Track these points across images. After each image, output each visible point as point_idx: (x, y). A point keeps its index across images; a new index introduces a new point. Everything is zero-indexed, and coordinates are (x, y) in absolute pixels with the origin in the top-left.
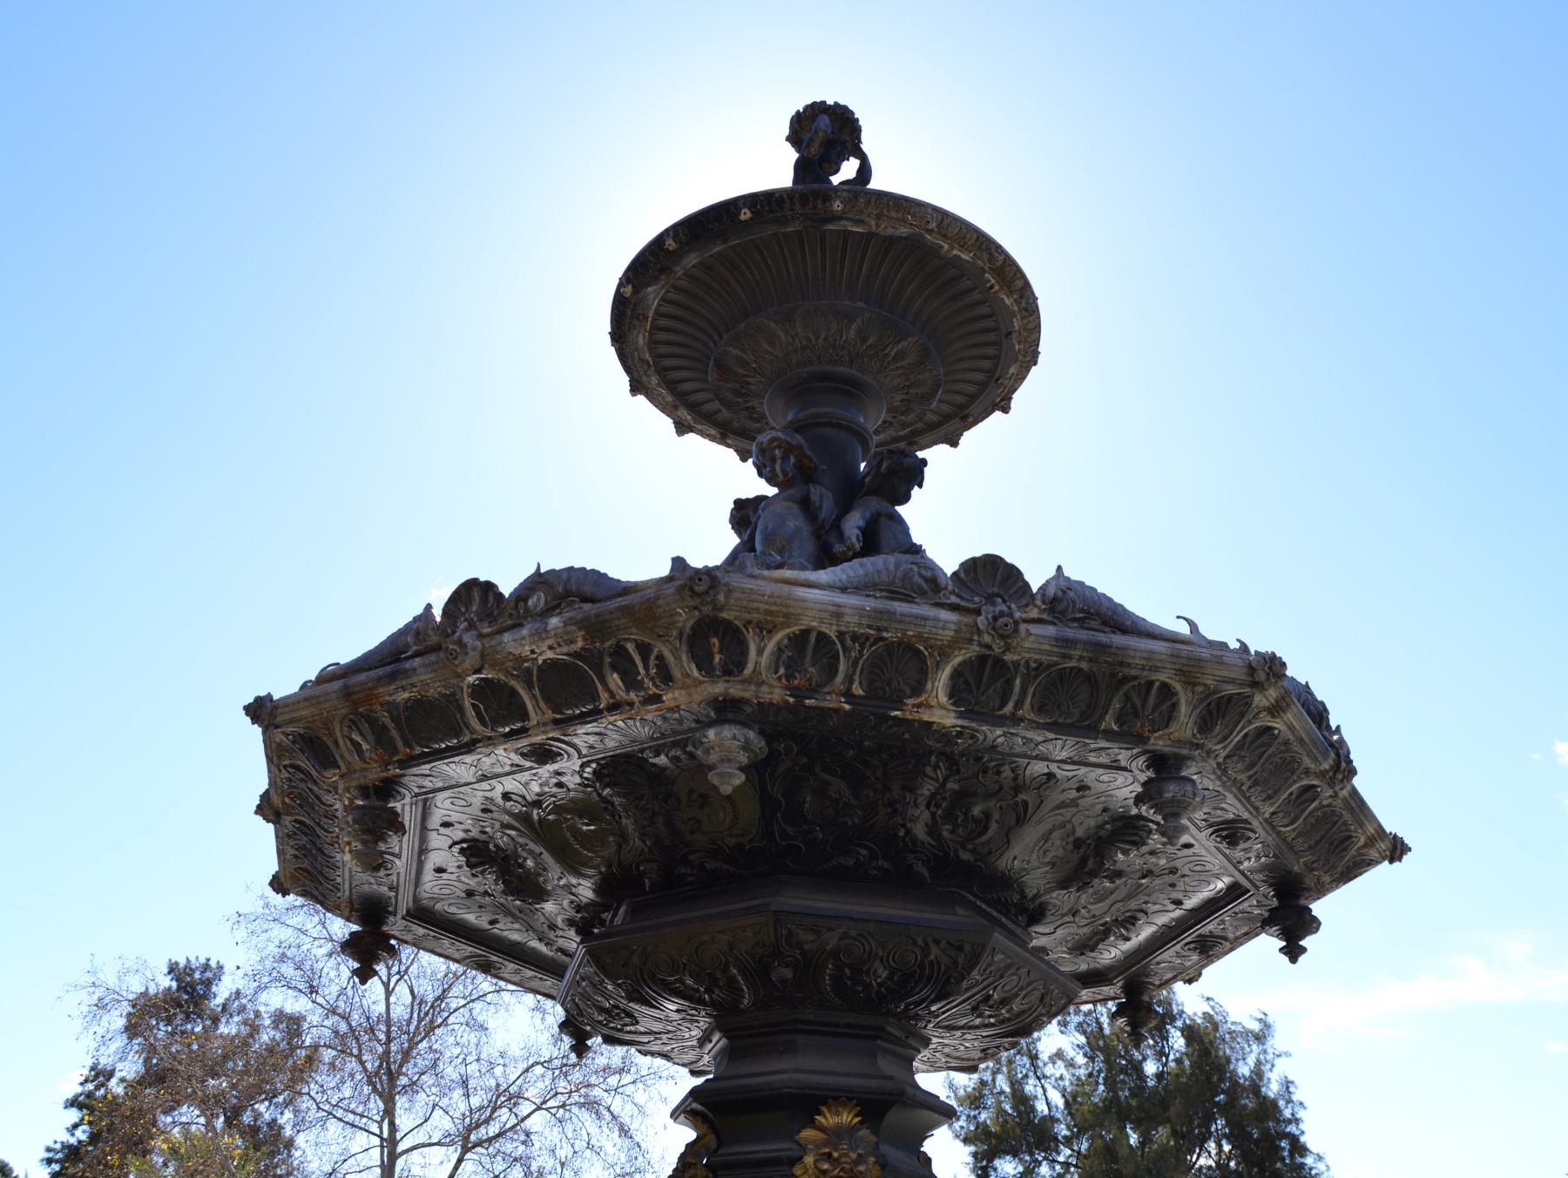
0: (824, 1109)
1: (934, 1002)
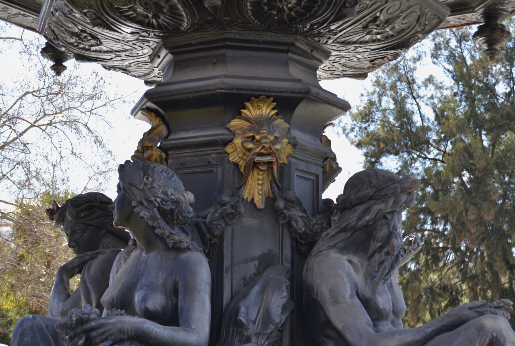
0: (248, 104)
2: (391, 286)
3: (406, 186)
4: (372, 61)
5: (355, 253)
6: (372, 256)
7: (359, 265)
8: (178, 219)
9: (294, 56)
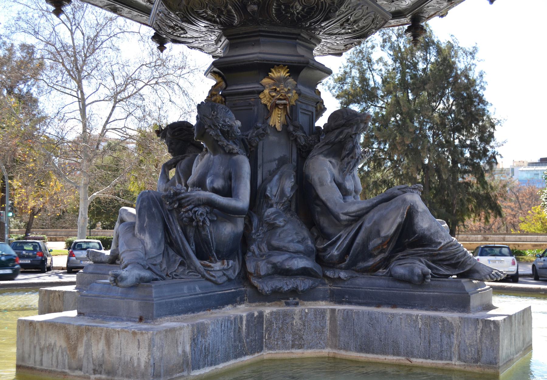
0: (273, 70)
1: (323, 21)
2: (354, 177)
3: (364, 118)
4: (345, 45)
5: (334, 157)
6: (343, 159)
7: (336, 165)
8: (232, 136)
9: (300, 42)
